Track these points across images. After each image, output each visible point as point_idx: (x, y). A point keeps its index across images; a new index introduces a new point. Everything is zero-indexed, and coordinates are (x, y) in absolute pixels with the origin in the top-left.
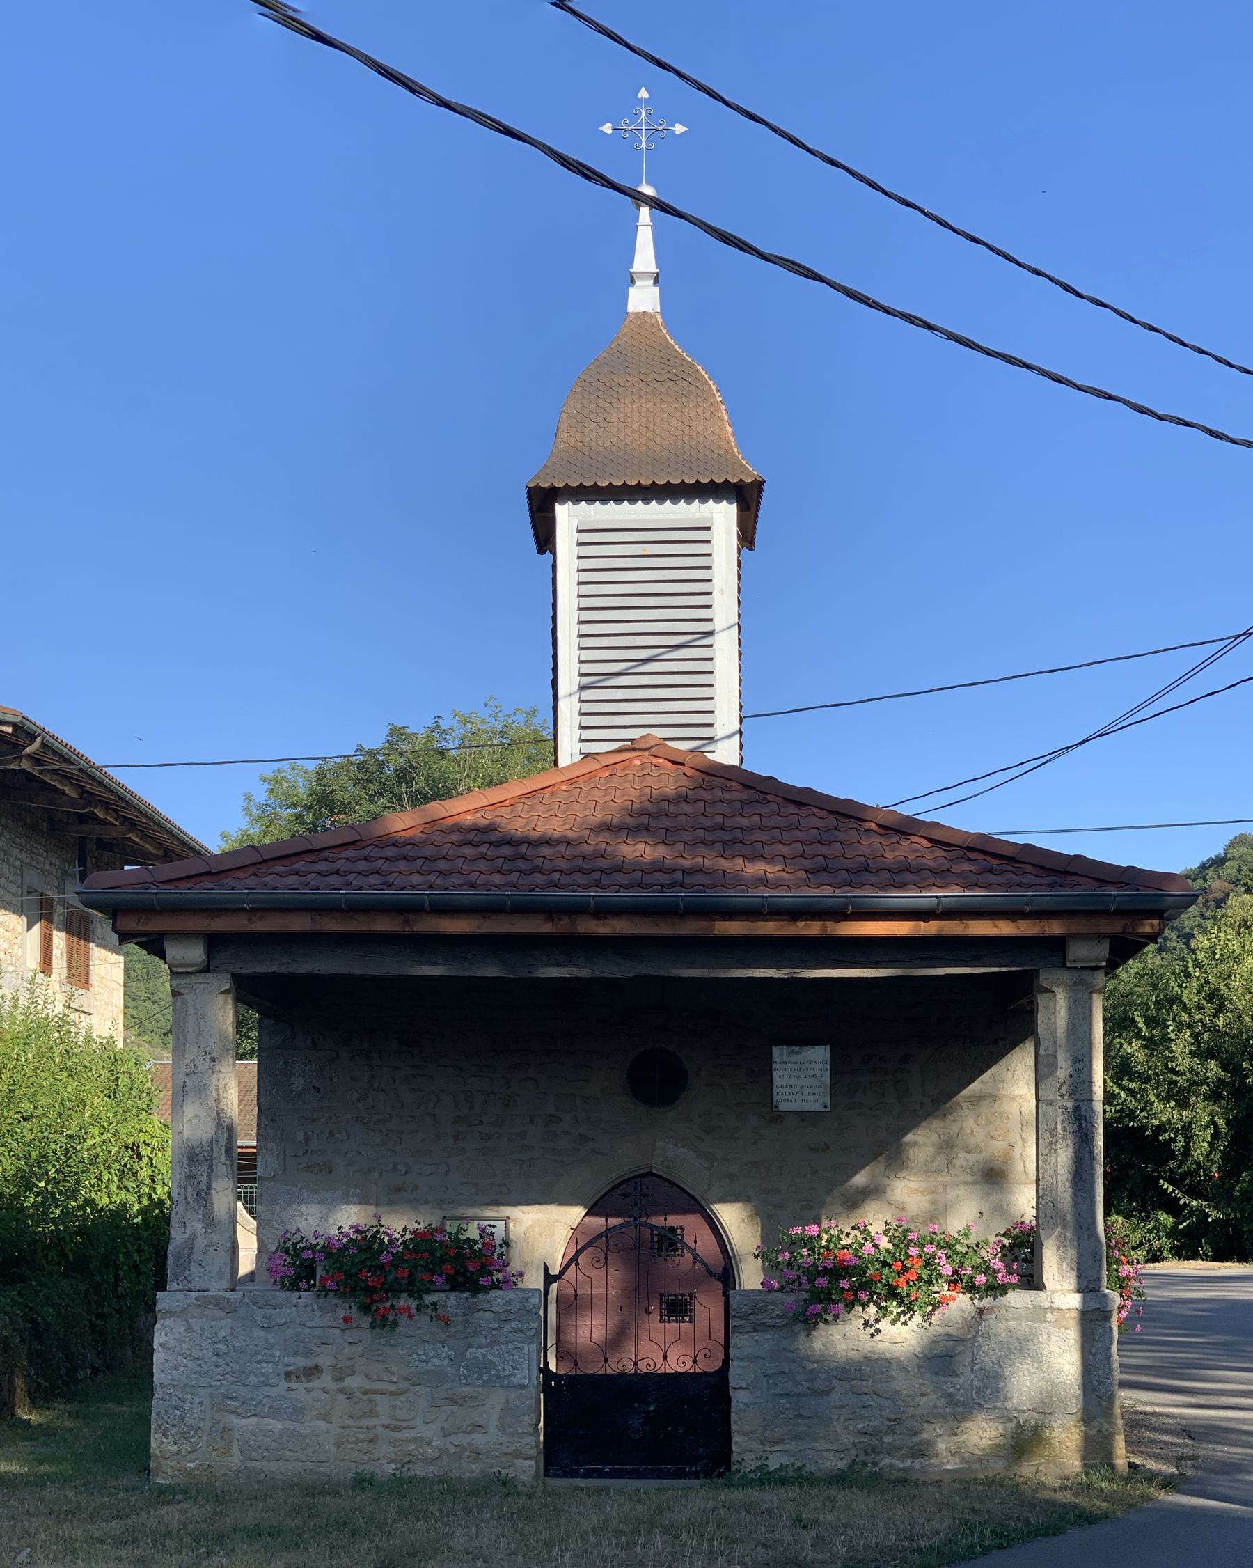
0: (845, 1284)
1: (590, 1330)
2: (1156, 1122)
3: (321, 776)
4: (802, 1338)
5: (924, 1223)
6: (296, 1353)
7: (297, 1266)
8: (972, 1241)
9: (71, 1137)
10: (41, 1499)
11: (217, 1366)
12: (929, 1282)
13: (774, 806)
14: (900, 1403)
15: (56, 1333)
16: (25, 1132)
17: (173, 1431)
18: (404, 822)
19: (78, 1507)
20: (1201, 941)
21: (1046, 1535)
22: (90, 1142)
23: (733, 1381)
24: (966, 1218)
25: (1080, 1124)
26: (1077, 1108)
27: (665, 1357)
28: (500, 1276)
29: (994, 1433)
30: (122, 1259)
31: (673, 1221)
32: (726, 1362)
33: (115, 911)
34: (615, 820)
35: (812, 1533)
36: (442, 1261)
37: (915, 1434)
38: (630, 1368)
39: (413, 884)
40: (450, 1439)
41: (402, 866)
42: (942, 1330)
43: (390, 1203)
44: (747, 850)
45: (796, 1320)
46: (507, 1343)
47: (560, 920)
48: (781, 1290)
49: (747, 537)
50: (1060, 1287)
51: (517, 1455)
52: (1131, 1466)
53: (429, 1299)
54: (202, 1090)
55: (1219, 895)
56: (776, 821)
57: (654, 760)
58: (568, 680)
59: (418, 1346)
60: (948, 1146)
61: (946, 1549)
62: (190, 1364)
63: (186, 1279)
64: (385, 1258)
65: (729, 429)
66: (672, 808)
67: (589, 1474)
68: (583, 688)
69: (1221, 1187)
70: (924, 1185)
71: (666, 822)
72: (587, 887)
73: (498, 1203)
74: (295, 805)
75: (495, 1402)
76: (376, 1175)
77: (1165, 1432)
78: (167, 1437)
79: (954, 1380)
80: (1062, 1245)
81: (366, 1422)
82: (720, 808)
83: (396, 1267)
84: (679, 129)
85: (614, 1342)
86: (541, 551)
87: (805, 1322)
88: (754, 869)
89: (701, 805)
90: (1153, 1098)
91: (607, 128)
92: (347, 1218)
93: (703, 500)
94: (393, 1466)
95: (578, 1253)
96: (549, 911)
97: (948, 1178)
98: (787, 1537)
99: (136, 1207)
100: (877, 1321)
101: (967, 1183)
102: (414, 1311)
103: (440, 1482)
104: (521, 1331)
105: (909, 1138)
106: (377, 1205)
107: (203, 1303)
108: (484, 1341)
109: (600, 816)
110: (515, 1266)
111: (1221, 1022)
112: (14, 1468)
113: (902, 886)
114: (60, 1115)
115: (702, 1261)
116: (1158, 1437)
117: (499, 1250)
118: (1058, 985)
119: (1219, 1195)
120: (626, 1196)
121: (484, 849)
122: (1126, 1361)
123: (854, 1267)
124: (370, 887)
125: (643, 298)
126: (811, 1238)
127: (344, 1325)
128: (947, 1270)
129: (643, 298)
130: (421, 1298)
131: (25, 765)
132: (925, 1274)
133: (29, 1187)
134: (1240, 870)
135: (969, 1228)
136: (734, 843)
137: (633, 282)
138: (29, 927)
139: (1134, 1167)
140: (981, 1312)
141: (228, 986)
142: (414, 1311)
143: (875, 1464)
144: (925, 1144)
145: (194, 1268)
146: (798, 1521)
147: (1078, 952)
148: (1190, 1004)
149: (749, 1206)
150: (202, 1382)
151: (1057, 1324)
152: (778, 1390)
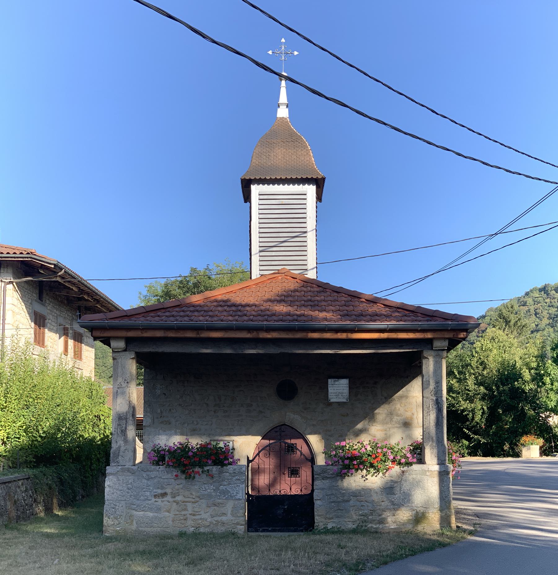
0: (355, 462)
1: (263, 480)
2: (462, 408)
3: (166, 285)
5: (382, 441)
6: (158, 488)
7: (159, 457)
8: (400, 447)
9: (75, 412)
10: (63, 542)
12: (385, 462)
13: (329, 293)
15: (69, 483)
16: (58, 410)
17: (112, 517)
18: (196, 299)
19: (76, 544)
20: (478, 345)
21: (428, 550)
22: (82, 414)
23: (315, 497)
24: (398, 440)
26: (437, 400)
27: (291, 489)
28: (231, 460)
30: (93, 456)
31: (293, 441)
32: (313, 491)
33: (92, 329)
34: (272, 298)
35: (344, 550)
36: (211, 455)
37: (380, 515)
38: (278, 493)
39: (201, 320)
41: (196, 314)
42: (389, 479)
43: (191, 435)
44: (319, 308)
45: (338, 476)
48: (332, 465)
49: (319, 198)
50: (431, 462)
51: (238, 524)
52: (458, 527)
53: (206, 468)
54: (123, 393)
55: (484, 329)
56: (330, 298)
57: (286, 277)
58: (255, 248)
59: (202, 485)
61: (392, 556)
62: (118, 492)
64: (190, 454)
65: (313, 159)
66: (293, 294)
67: (263, 531)
68: (260, 251)
69: (485, 431)
70: (382, 428)
71: (290, 299)
72: (263, 321)
73: (229, 435)
74: (157, 296)
76: (186, 425)
77: (469, 515)
78: (109, 519)
79: (394, 496)
80: (432, 448)
81: (183, 513)
82: (309, 293)
83: (194, 457)
84: (296, 53)
85: (272, 484)
86: (246, 202)
87: (341, 476)
88: (322, 315)
89: (303, 292)
90: (461, 400)
91: (270, 52)
92: (175, 440)
93: (304, 184)
95: (259, 452)
96: (249, 329)
97: (391, 426)
98: (335, 552)
99: (99, 438)
100: (366, 475)
101: (397, 427)
102: (201, 473)
103: (210, 534)
104: (239, 480)
105: (377, 411)
106: (187, 435)
107: (123, 470)
108: (226, 483)
109: (267, 296)
110: (236, 457)
111: (485, 372)
112: (53, 531)
113: (375, 321)
114: (71, 404)
115: (304, 455)
116: (466, 517)
117: (231, 451)
118: (430, 356)
119: (485, 433)
120: (276, 432)
121: (226, 308)
122: (455, 491)
123: (358, 456)
124: (185, 321)
125: (283, 112)
126: (343, 446)
127: (176, 478)
128: (391, 457)
129: (283, 112)
130: (203, 468)
131: (58, 279)
132: (383, 459)
133: (59, 430)
134: (491, 320)
135: (399, 442)
136: (315, 306)
137: (279, 106)
138: (60, 338)
139: (456, 424)
140: (403, 472)
141: (133, 356)
142: (201, 473)
144: (382, 414)
146: (339, 546)
147: (437, 344)
148: (474, 366)
149: (320, 436)
150: (122, 499)
152: (331, 500)
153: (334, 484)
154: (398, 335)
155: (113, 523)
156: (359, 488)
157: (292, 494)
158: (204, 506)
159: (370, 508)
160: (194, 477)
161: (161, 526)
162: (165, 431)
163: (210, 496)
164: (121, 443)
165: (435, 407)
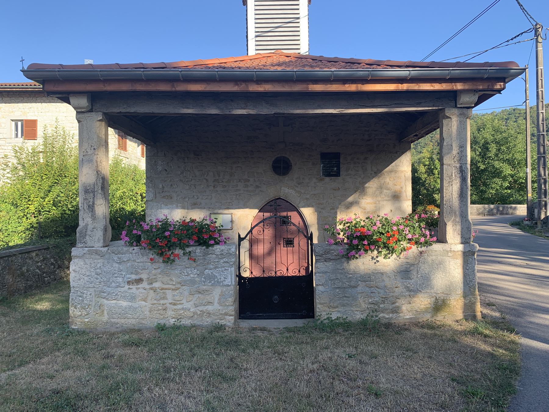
4: (345, 264)
6: (132, 273)
11: (97, 279)
14: (387, 291)
25: (462, 174)
26: (461, 167)
27: (287, 270)
29: (426, 303)
31: (289, 214)
38: (273, 274)
40: (198, 308)
42: (405, 261)
46: (222, 267)
47: (241, 85)
51: (226, 314)
53: (188, 250)
54: (90, 161)
58: (252, 34)
59: (183, 270)
60: (381, 188)
62: (86, 278)
63: (84, 242)
70: (372, 201)
73: (228, 208)
75: (217, 292)
76: (187, 199)
78: (76, 309)
79: (410, 281)
81: (162, 302)
94: (174, 320)
100: (377, 257)
105: (367, 185)
107: (90, 253)
108: (212, 267)
120: (271, 206)
130: (184, 249)
140: (421, 253)
141: (101, 118)
143: (376, 316)
144: (372, 188)
145: (87, 237)
147: (465, 99)
150: (90, 285)
151: (454, 257)
153: (338, 266)
154: (419, 86)
155: (80, 313)
156: (370, 272)
157: (289, 275)
158: (186, 293)
159: (381, 295)
160: (174, 261)
161: (136, 317)
162: (166, 205)
163: (193, 282)
164: (89, 220)
165: (458, 176)
